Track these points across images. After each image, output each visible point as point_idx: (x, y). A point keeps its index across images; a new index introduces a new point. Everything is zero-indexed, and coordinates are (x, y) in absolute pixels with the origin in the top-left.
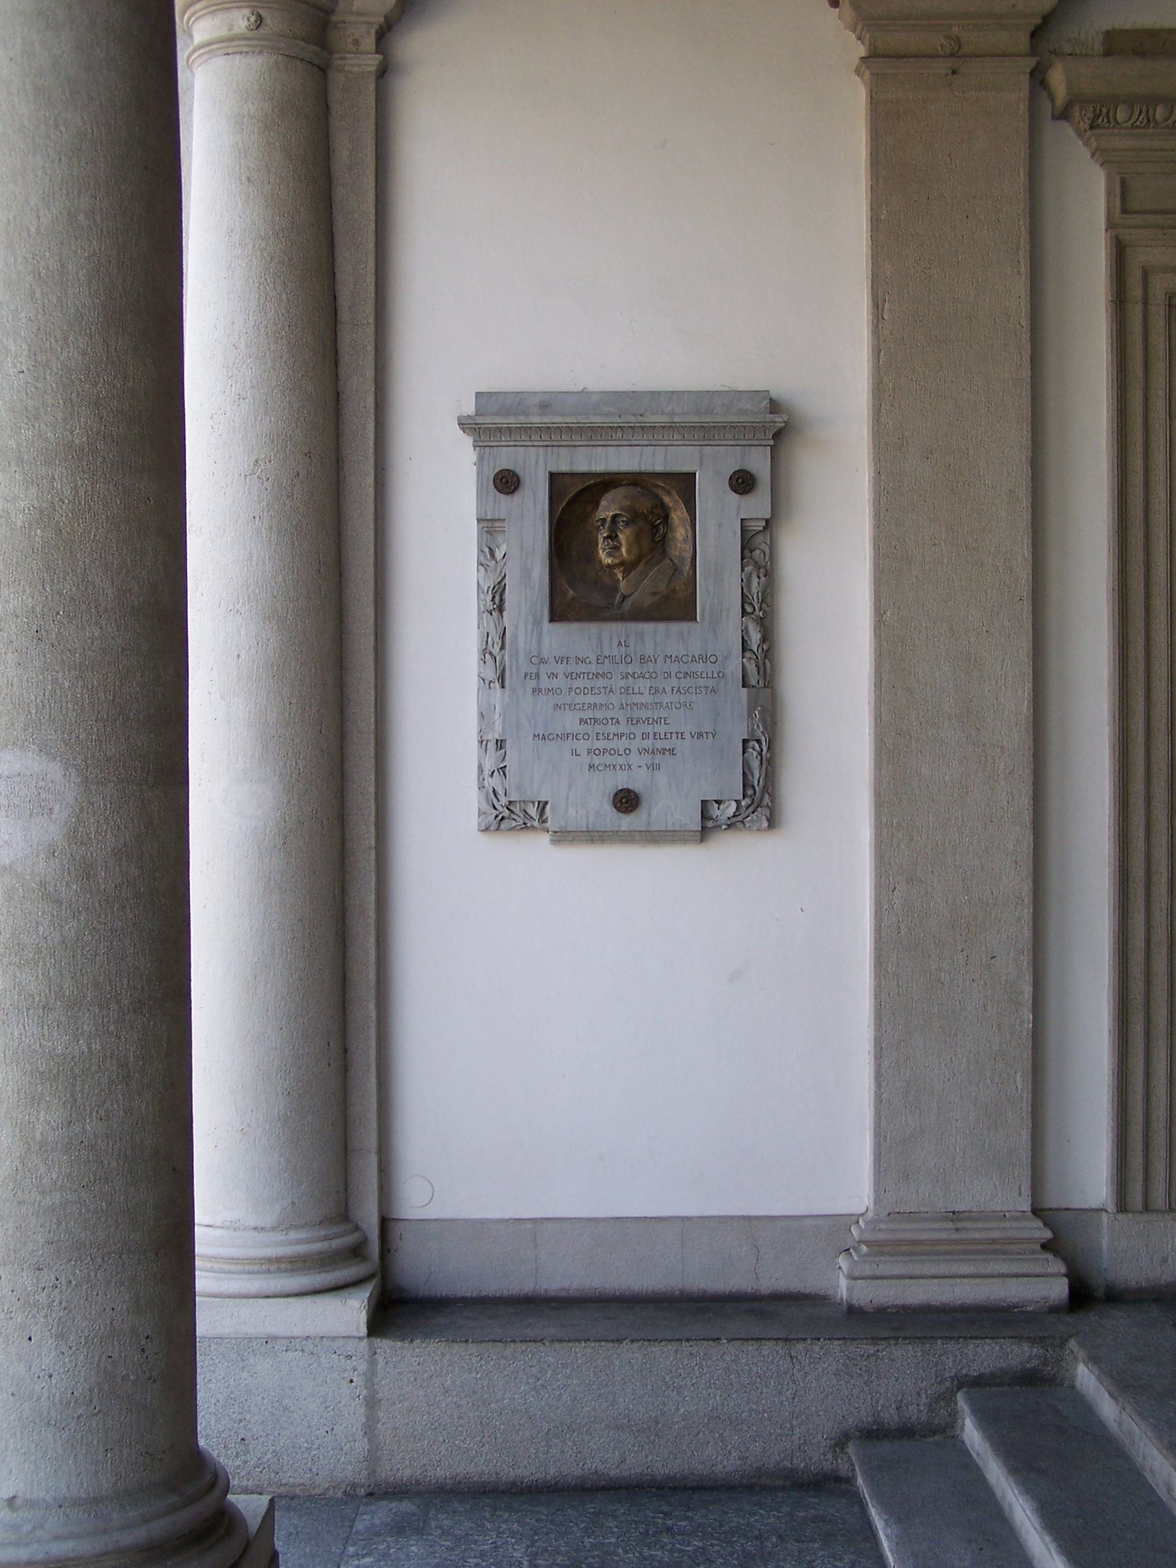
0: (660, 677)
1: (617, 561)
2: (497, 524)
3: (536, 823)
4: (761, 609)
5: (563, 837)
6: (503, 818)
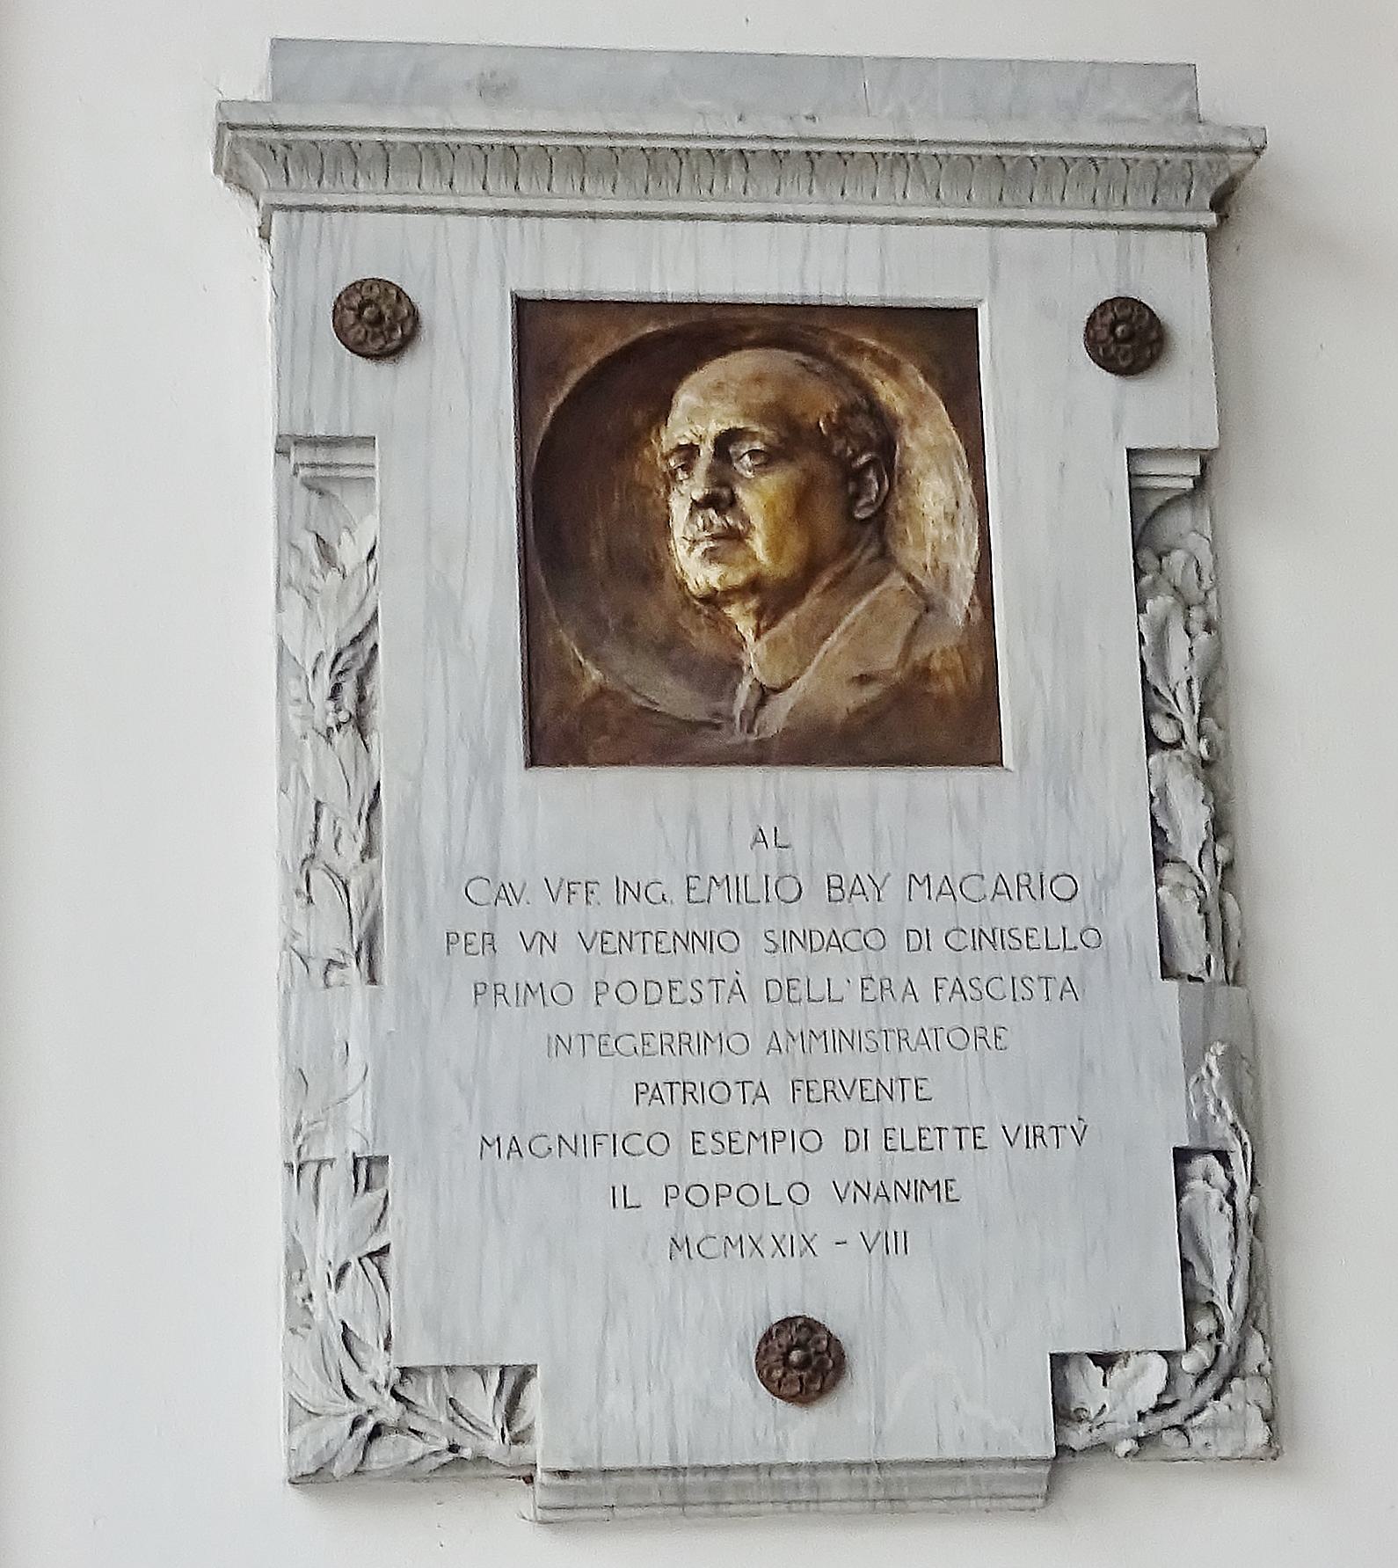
0: (896, 944)
1: (738, 578)
2: (346, 456)
3: (493, 1446)
4: (1194, 724)
5: (589, 1493)
6: (377, 1432)
